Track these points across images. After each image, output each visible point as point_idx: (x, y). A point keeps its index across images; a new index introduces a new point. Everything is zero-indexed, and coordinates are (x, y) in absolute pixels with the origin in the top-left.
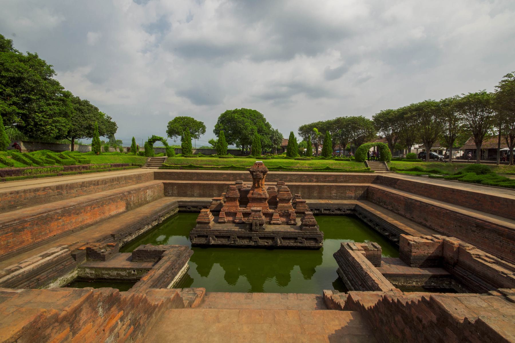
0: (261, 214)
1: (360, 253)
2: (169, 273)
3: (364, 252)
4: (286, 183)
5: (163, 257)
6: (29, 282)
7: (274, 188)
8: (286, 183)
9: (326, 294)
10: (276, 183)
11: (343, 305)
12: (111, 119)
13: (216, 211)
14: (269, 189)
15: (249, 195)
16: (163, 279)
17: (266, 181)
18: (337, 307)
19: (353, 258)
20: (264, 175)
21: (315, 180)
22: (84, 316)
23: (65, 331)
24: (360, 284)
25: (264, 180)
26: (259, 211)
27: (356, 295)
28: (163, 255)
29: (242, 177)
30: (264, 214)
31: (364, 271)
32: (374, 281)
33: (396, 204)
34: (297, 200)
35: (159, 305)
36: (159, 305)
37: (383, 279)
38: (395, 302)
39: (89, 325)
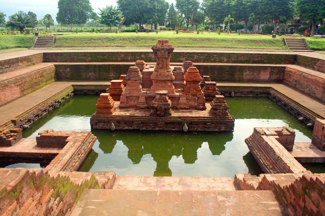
0: (167, 98)
1: (273, 138)
2: (76, 157)
3: (277, 137)
4: (194, 64)
5: (67, 142)
6: (220, 119)
7: (180, 69)
8: (194, 64)
9: (238, 177)
10: (182, 64)
11: (256, 187)
12: (222, 3)
13: (116, 95)
14: (175, 70)
15: (152, 77)
16: (71, 163)
17: (171, 62)
18: (251, 188)
19: (267, 143)
20: (169, 53)
21: (225, 60)
22: (26, 192)
23: (14, 204)
24: (271, 167)
25: (169, 60)
26: (165, 95)
27: (270, 177)
28: (67, 140)
29: (143, 56)
30: (170, 98)
31: (277, 155)
32: (286, 164)
33: (314, 87)
34: (206, 82)
35: (80, 185)
36: (80, 185)
37: (296, 162)
38: (313, 181)
39: (30, 199)
